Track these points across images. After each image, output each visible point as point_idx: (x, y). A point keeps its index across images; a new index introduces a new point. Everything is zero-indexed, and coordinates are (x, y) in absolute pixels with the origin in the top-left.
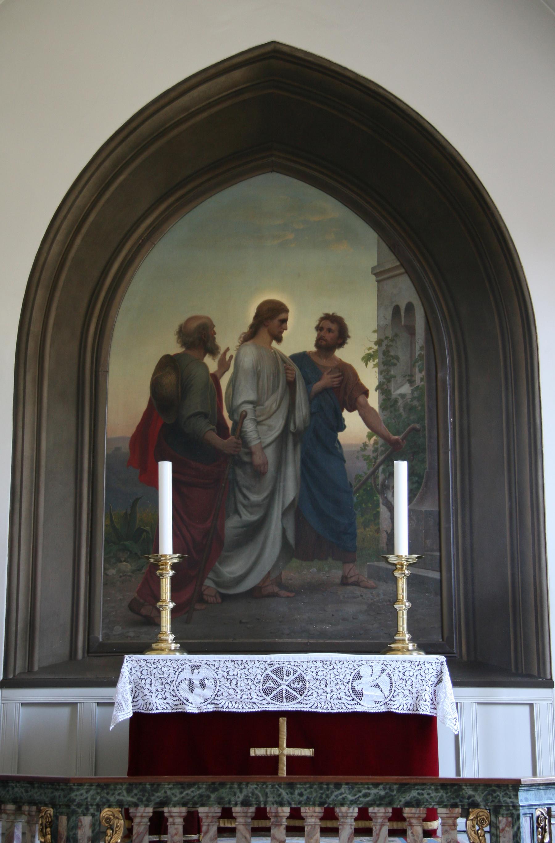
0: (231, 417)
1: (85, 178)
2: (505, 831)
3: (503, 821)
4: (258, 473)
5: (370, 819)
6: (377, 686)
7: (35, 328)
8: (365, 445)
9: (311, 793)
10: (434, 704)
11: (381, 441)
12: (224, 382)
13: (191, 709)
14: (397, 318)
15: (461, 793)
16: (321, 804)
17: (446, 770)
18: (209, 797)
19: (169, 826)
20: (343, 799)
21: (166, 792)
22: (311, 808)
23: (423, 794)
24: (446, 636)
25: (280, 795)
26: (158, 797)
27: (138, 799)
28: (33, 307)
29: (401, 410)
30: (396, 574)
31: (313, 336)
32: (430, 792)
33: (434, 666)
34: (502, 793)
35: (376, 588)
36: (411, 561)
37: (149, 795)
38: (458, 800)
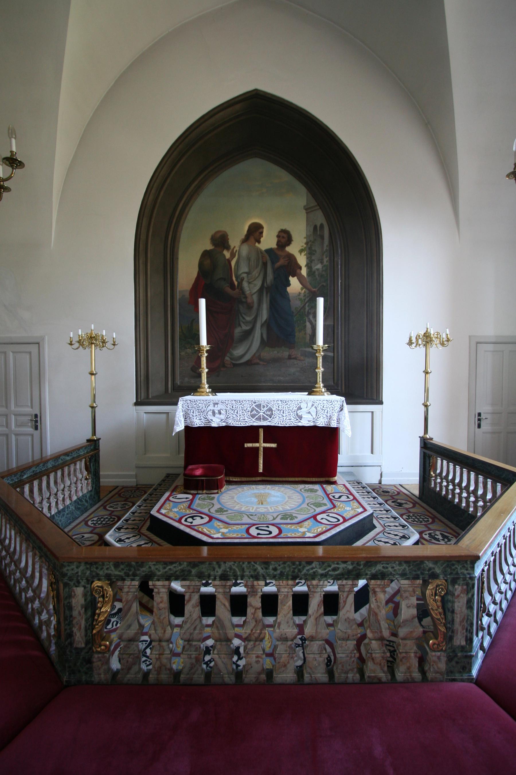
0: (236, 280)
1: (165, 161)
2: (460, 597)
3: (458, 589)
4: (250, 307)
6: (309, 413)
7: (143, 237)
8: (300, 293)
9: (285, 568)
10: (338, 421)
11: (307, 291)
12: (233, 263)
13: (214, 425)
14: (315, 232)
15: (422, 566)
18: (190, 572)
19: (155, 595)
20: (314, 572)
21: (150, 567)
22: (284, 582)
23: (387, 568)
24: (335, 381)
25: (255, 570)
26: (143, 571)
27: (125, 573)
28: (141, 227)
29: (317, 276)
30: (317, 355)
31: (275, 240)
32: (394, 565)
33: (339, 403)
34: (460, 566)
35: (303, 360)
36: (324, 348)
37: (135, 570)
38: (419, 572)
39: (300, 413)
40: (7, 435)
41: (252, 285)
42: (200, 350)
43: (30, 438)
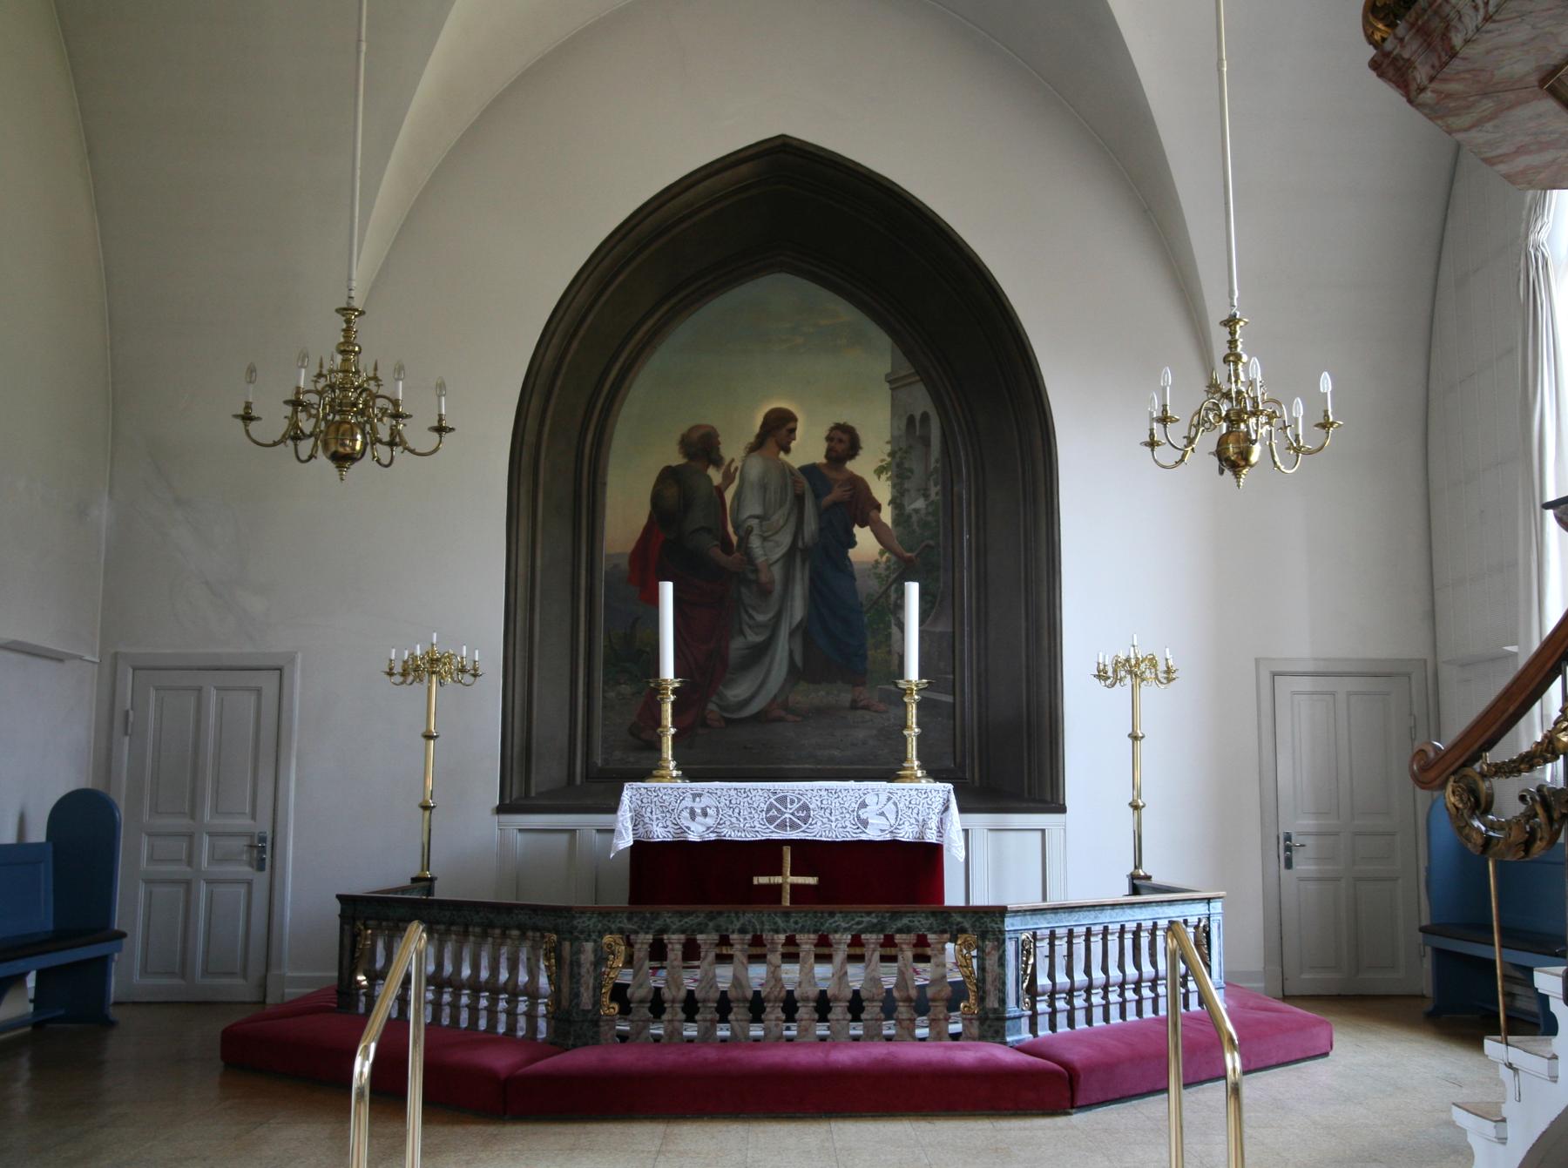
0: (736, 533)
3: (989, 945)
4: (765, 592)
5: (895, 945)
6: (882, 814)
7: (530, 438)
8: (877, 562)
11: (894, 559)
12: (729, 495)
13: (693, 837)
14: (911, 431)
16: (815, 932)
17: (953, 896)
39: (864, 814)
40: (188, 884)
41: (769, 544)
42: (658, 689)
43: (243, 890)
